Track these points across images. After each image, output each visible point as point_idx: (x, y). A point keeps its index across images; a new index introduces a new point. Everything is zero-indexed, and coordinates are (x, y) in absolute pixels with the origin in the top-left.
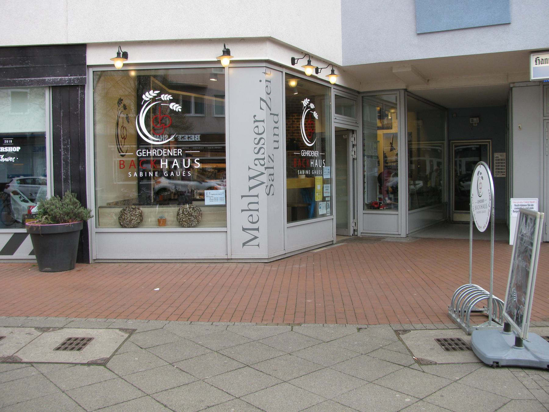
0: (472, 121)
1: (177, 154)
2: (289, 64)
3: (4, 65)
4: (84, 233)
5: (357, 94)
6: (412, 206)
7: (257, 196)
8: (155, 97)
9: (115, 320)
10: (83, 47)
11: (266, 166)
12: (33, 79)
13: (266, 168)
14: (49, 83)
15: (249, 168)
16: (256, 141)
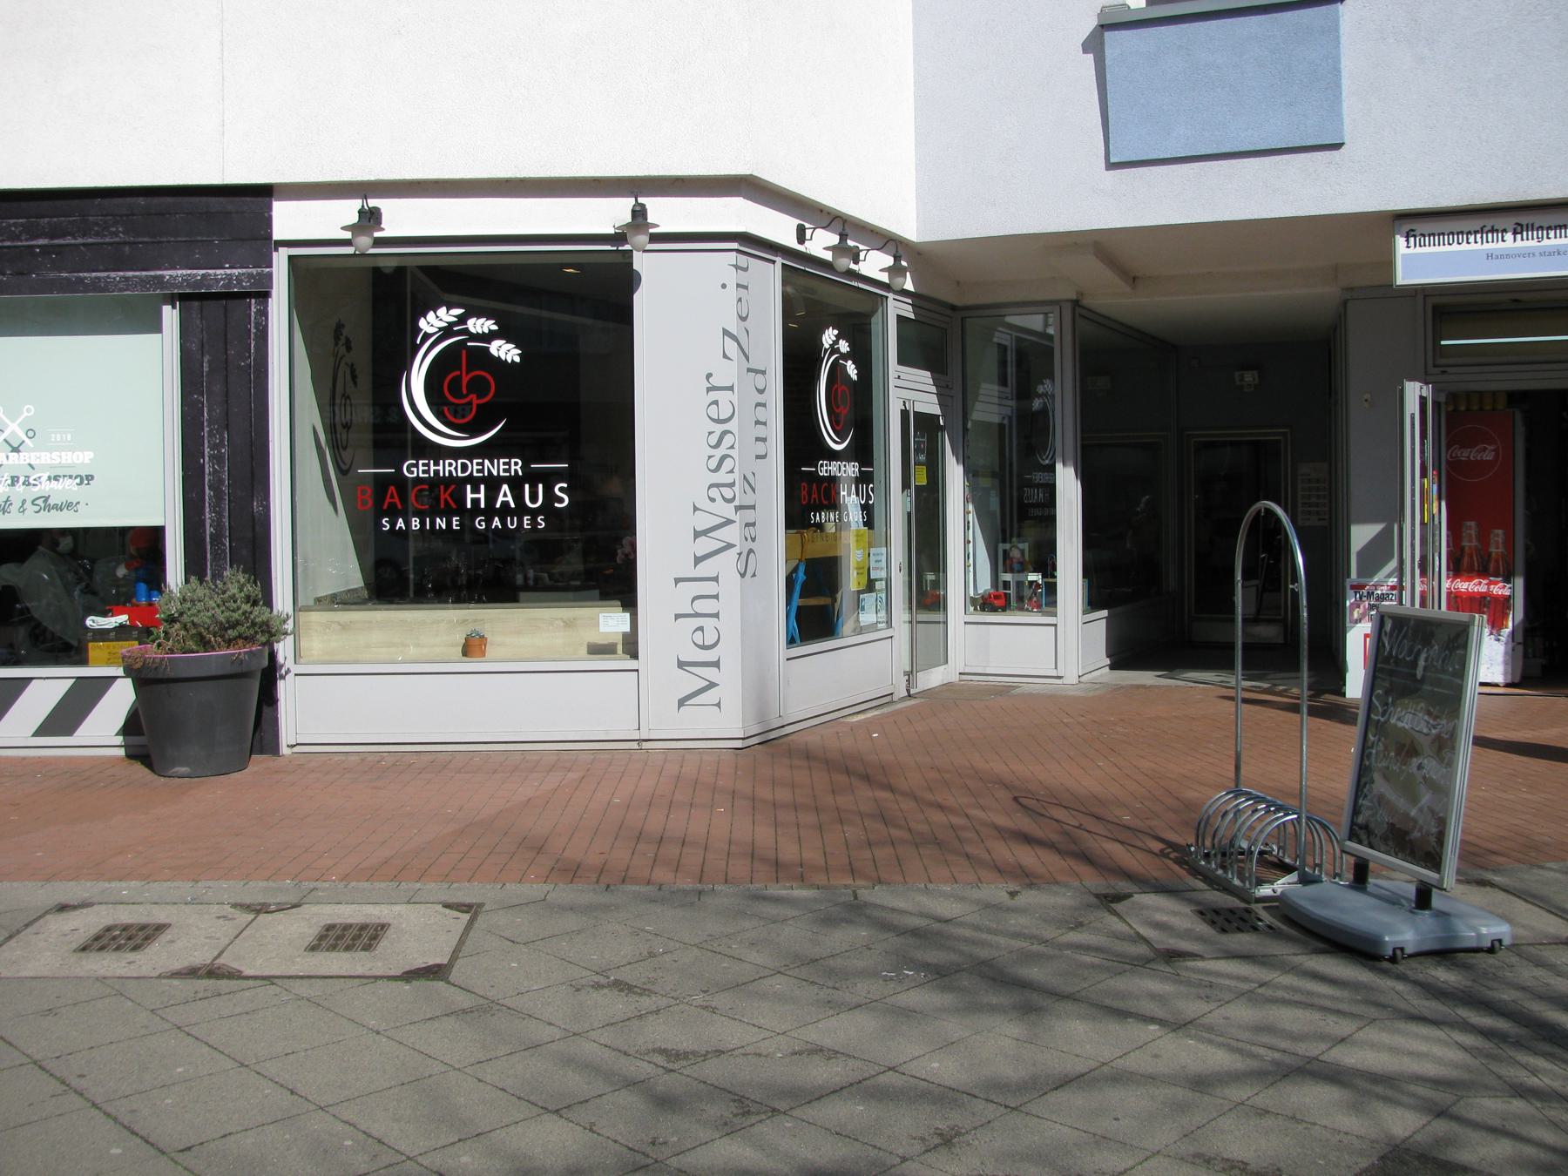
0: (1242, 379)
1: (508, 470)
2: (791, 241)
3: (52, 238)
4: (270, 675)
5: (949, 312)
6: (1094, 601)
7: (716, 579)
8: (451, 325)
9: (418, 885)
10: (265, 193)
11: (737, 503)
12: (130, 274)
13: (738, 508)
14: (174, 286)
15: (696, 509)
16: (714, 440)
